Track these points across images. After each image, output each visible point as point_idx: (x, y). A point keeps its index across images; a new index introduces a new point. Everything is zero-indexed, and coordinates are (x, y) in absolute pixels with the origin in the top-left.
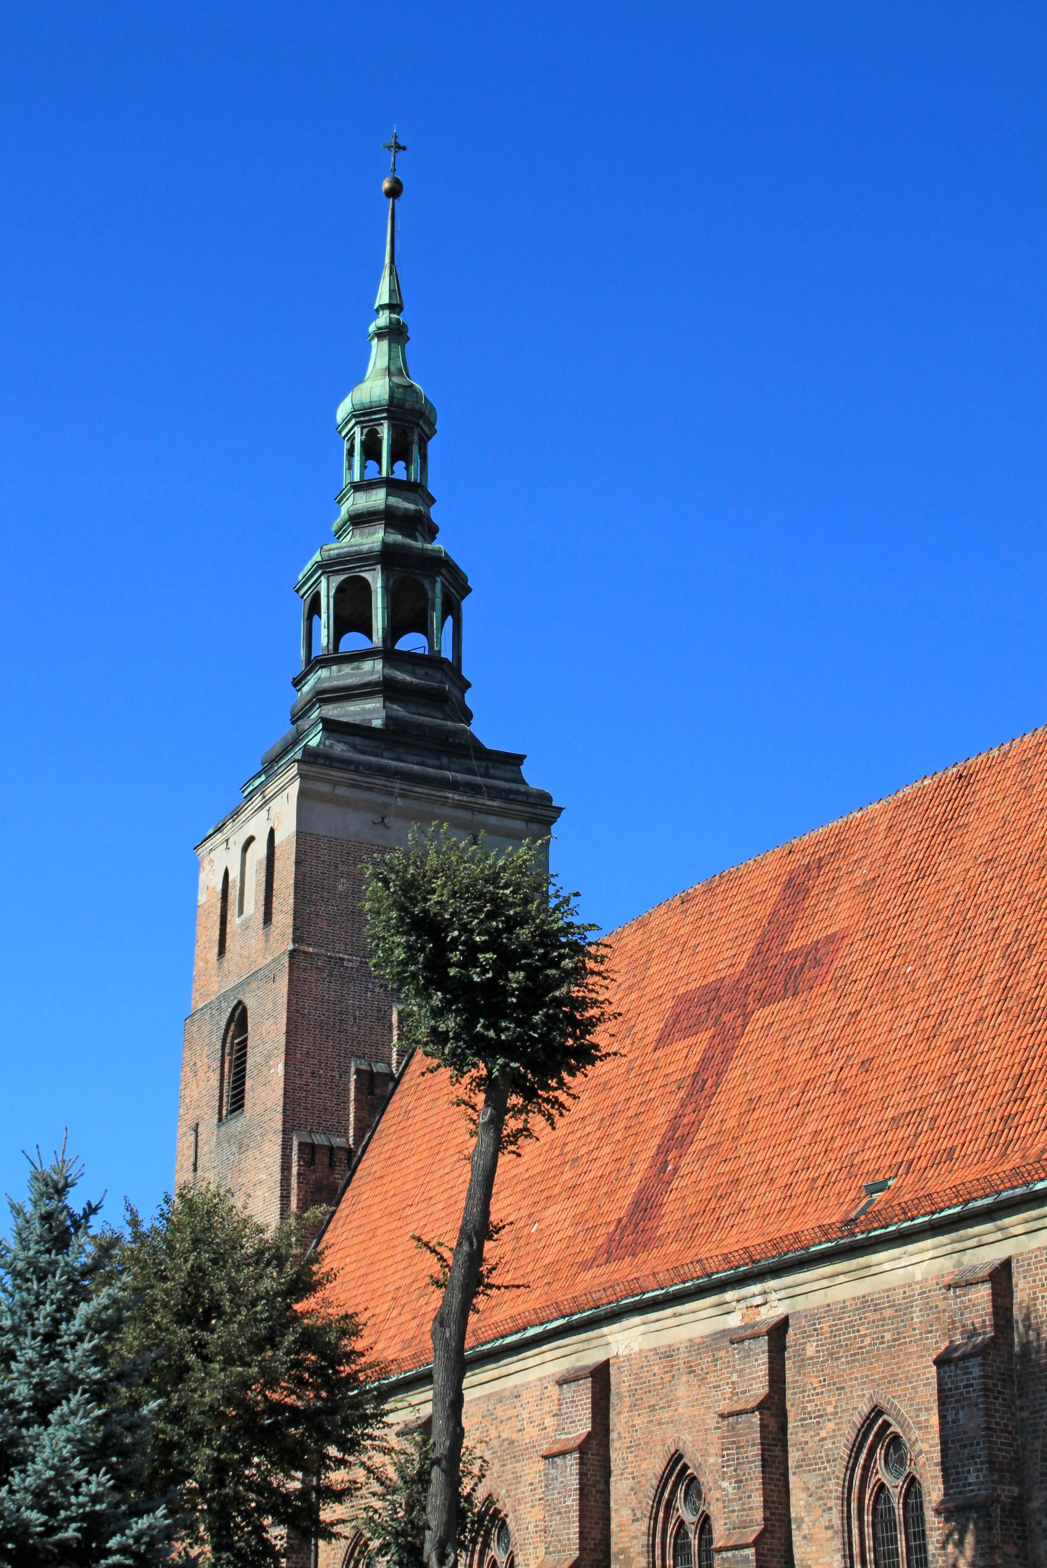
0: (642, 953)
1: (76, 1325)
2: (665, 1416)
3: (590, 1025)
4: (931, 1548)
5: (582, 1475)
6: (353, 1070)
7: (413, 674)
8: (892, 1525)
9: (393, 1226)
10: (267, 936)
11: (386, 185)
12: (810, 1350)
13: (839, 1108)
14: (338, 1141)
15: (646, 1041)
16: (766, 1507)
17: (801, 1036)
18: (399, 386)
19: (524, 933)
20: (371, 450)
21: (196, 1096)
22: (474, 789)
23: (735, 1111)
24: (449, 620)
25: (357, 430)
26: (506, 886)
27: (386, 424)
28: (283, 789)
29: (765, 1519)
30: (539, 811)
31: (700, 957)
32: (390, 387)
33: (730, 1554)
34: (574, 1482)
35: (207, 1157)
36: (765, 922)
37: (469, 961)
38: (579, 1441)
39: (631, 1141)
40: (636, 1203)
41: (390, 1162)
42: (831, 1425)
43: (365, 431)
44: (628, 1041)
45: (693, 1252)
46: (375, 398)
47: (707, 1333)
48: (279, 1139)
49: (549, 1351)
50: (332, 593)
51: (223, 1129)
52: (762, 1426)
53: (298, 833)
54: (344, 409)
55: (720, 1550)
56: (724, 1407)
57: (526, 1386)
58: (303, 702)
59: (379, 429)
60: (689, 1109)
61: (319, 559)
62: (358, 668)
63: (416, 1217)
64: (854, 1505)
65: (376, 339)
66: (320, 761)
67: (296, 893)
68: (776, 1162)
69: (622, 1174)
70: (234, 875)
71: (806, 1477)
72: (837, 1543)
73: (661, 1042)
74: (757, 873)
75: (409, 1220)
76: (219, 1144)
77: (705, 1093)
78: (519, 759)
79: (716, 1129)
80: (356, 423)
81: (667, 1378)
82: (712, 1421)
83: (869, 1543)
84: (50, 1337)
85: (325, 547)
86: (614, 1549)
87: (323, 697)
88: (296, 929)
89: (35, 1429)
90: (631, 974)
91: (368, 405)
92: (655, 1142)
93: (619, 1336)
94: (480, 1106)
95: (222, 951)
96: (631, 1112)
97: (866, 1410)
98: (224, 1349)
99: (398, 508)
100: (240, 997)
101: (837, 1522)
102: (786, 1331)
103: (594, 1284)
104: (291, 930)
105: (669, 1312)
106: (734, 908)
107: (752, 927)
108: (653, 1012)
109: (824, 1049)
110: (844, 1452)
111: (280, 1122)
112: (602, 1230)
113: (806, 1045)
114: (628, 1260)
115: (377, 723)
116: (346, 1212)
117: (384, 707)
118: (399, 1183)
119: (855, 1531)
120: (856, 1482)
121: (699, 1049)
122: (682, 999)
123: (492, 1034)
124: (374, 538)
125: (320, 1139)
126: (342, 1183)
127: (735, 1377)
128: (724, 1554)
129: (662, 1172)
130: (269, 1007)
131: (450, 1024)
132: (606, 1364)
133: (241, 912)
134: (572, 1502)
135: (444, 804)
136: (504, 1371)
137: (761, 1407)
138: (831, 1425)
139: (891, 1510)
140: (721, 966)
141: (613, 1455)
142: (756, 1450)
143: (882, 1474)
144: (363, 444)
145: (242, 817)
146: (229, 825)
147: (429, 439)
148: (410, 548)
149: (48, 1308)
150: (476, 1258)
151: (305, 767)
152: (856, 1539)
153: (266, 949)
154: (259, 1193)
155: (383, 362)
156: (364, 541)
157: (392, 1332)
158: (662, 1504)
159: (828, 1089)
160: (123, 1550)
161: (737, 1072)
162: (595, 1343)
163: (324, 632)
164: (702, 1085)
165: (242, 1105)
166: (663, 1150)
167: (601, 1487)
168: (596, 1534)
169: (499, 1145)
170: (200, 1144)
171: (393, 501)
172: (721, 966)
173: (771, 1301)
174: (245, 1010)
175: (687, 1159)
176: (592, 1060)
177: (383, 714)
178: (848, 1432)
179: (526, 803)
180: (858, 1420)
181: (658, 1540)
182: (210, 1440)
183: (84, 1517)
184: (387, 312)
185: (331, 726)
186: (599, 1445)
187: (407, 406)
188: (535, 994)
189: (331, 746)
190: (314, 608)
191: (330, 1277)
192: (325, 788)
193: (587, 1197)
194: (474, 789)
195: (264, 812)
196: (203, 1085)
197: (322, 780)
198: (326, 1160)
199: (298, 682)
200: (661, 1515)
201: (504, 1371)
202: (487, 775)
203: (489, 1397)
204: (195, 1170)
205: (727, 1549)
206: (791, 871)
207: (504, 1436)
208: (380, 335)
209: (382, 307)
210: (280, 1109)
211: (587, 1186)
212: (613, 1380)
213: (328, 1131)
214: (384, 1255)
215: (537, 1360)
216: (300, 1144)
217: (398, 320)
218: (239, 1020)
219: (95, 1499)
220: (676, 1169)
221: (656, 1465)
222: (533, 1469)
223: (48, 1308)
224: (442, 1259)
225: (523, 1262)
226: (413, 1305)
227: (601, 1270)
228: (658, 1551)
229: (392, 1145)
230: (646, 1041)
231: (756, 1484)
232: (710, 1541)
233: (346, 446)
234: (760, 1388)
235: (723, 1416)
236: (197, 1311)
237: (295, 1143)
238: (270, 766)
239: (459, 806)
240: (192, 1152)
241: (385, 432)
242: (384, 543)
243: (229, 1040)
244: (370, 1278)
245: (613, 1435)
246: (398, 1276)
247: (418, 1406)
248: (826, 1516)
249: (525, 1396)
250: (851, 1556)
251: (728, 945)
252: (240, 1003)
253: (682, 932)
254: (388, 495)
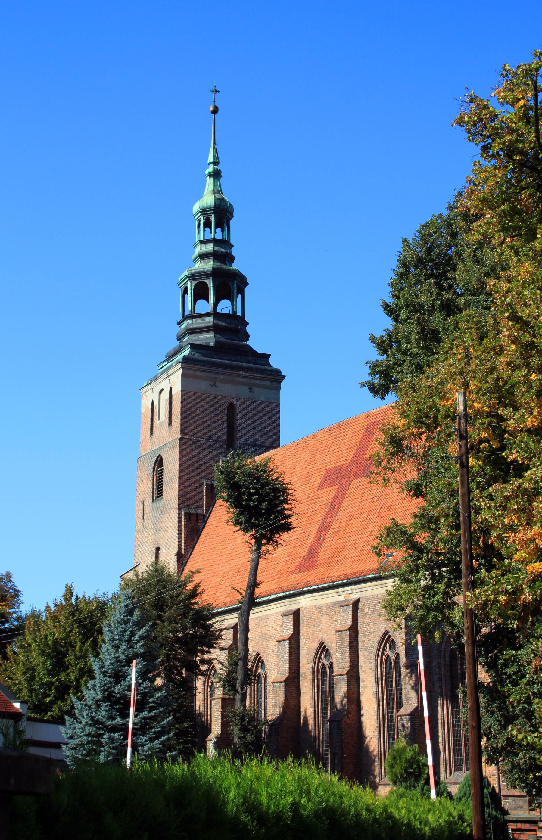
0: (314, 449)
1: (137, 638)
2: (318, 629)
3: (289, 516)
4: (402, 677)
5: (290, 648)
6: (205, 483)
7: (225, 322)
8: (391, 668)
9: (222, 547)
10: (170, 430)
11: (211, 109)
12: (366, 610)
13: (379, 523)
14: (199, 512)
15: (315, 486)
16: (350, 662)
17: (368, 493)
18: (218, 199)
19: (267, 489)
20: (207, 224)
21: (143, 490)
22: (250, 370)
23: (345, 519)
24: (240, 296)
25: (201, 217)
26: (261, 471)
27: (213, 216)
28: (175, 372)
29: (350, 666)
30: (276, 378)
31: (335, 455)
32: (215, 200)
33: (338, 677)
34: (287, 650)
35: (148, 514)
36: (358, 444)
37: (249, 499)
38: (289, 636)
39: (308, 526)
40: (310, 551)
41: (219, 521)
42: (372, 636)
43: (205, 218)
44: (308, 485)
45: (329, 572)
46: (208, 204)
47: (333, 601)
48: (177, 511)
49: (278, 604)
50: (193, 288)
51: (154, 504)
52: (349, 635)
53: (182, 391)
54: (196, 208)
55: (335, 676)
56: (338, 628)
57: (271, 615)
58: (182, 333)
59: (210, 217)
60: (329, 516)
61: (187, 274)
62: (204, 320)
63: (230, 545)
64: (379, 662)
65: (208, 177)
66: (190, 362)
67: (181, 415)
68: (357, 541)
69: (305, 538)
70: (156, 403)
71: (364, 652)
72: (374, 674)
73: (320, 487)
74: (356, 423)
75: (227, 546)
76: (153, 510)
77: (335, 510)
78: (269, 356)
79: (337, 525)
80: (201, 215)
81: (319, 616)
82: (334, 632)
83: (384, 674)
84: (129, 641)
85: (190, 269)
86: (301, 672)
87: (190, 331)
88: (181, 429)
89: (127, 668)
90: (310, 457)
91: (205, 207)
92: (317, 527)
93: (303, 600)
94: (253, 544)
95: (152, 433)
96: (309, 514)
97: (383, 631)
98: (169, 618)
99: (218, 251)
100: (160, 453)
101: (373, 667)
102: (358, 603)
103: (295, 580)
104: (180, 429)
105: (320, 593)
106: (347, 436)
107: (353, 445)
108: (317, 475)
109: (376, 499)
110: (376, 645)
111: (177, 505)
112: (298, 560)
113: (370, 497)
114: (306, 572)
115: (212, 344)
116: (203, 539)
117: (215, 337)
118: (223, 530)
119: (379, 670)
120: (380, 654)
121: (334, 492)
122: (328, 471)
123: (257, 522)
124: (209, 265)
125: (192, 511)
126: (201, 527)
127: (341, 618)
128: (337, 677)
129: (319, 540)
130: (172, 459)
131: (243, 519)
132: (298, 610)
133: (159, 419)
134: (287, 657)
135: (239, 376)
136: (263, 609)
137: (349, 629)
138: (372, 636)
139: (391, 663)
140: (342, 460)
141: (301, 641)
142: (348, 643)
143: (388, 652)
144: (204, 223)
145: (159, 381)
146: (153, 383)
147: (231, 219)
148: (224, 269)
149: (128, 633)
150: (252, 594)
151: (184, 365)
152: (379, 673)
153: (170, 435)
154: (169, 531)
155: (211, 187)
156: (206, 267)
157: (222, 590)
158: (317, 658)
159: (376, 515)
160: (153, 702)
161: (346, 504)
162: (295, 602)
163: (190, 304)
164: (334, 507)
165: (162, 495)
166: (320, 531)
167: (297, 652)
168: (295, 668)
169: (260, 557)
170: (145, 509)
171: (216, 248)
172: (342, 460)
173: (354, 593)
174: (162, 459)
175: (328, 536)
176: (290, 529)
177: (214, 340)
178: (378, 639)
179: (271, 375)
180: (381, 635)
181: (316, 670)
182: (165, 648)
183: (142, 693)
184: (213, 165)
185: (193, 346)
186: (296, 638)
187: (222, 207)
188: (271, 510)
189: (194, 355)
190: (185, 291)
191: (202, 592)
192: (192, 372)
193: (292, 546)
194: (250, 370)
195: (168, 380)
196: (146, 486)
197: (191, 369)
198: (195, 519)
199: (179, 323)
200: (317, 662)
201: (263, 609)
202: (255, 363)
203: (258, 618)
204: (143, 519)
205: (337, 675)
206: (368, 424)
207: (263, 632)
208: (210, 176)
209: (211, 163)
210: (177, 500)
211: (292, 542)
212: (301, 615)
213: (195, 507)
214: (218, 559)
215: (275, 606)
216: (185, 513)
217: (217, 169)
218: (159, 462)
219: (145, 688)
220: (324, 539)
221: (316, 645)
222: (273, 644)
223: (128, 633)
224: (241, 594)
225: (269, 568)
226: (229, 580)
227: (297, 575)
228: (316, 674)
229: (220, 514)
230: (315, 486)
231: (348, 654)
232: (333, 671)
233: (197, 223)
234: (349, 623)
235: (337, 632)
236: (160, 605)
237: (183, 513)
238: (170, 357)
239: (244, 377)
240: (142, 512)
241: (213, 219)
242: (213, 268)
243: (156, 469)
244: (213, 567)
245: (301, 634)
246: (224, 568)
247: (232, 619)
248: (370, 665)
249: (270, 619)
250: (378, 678)
251: (345, 451)
252: (160, 455)
253: (328, 443)
254: (214, 246)
